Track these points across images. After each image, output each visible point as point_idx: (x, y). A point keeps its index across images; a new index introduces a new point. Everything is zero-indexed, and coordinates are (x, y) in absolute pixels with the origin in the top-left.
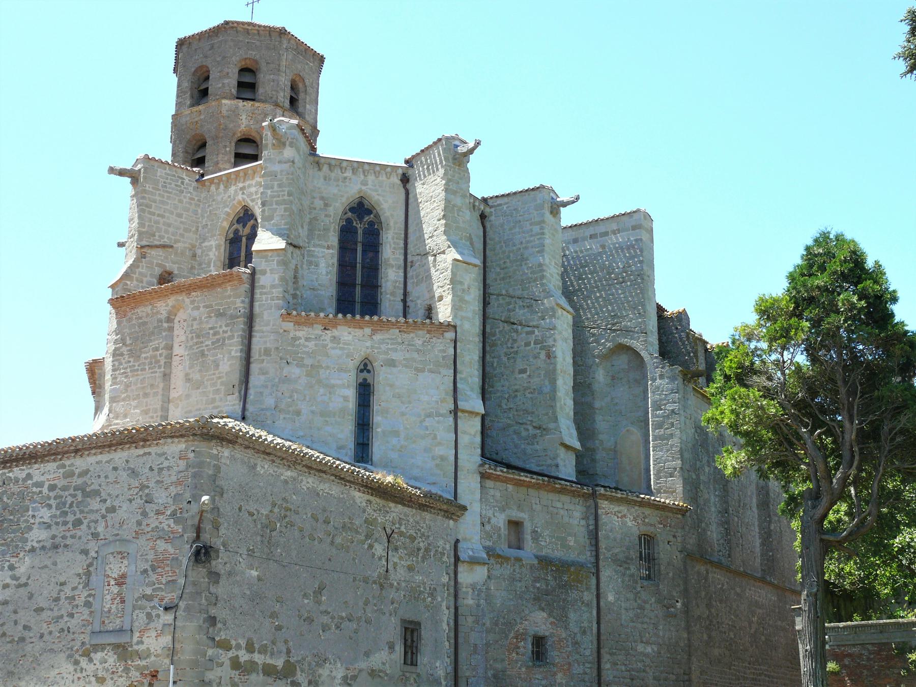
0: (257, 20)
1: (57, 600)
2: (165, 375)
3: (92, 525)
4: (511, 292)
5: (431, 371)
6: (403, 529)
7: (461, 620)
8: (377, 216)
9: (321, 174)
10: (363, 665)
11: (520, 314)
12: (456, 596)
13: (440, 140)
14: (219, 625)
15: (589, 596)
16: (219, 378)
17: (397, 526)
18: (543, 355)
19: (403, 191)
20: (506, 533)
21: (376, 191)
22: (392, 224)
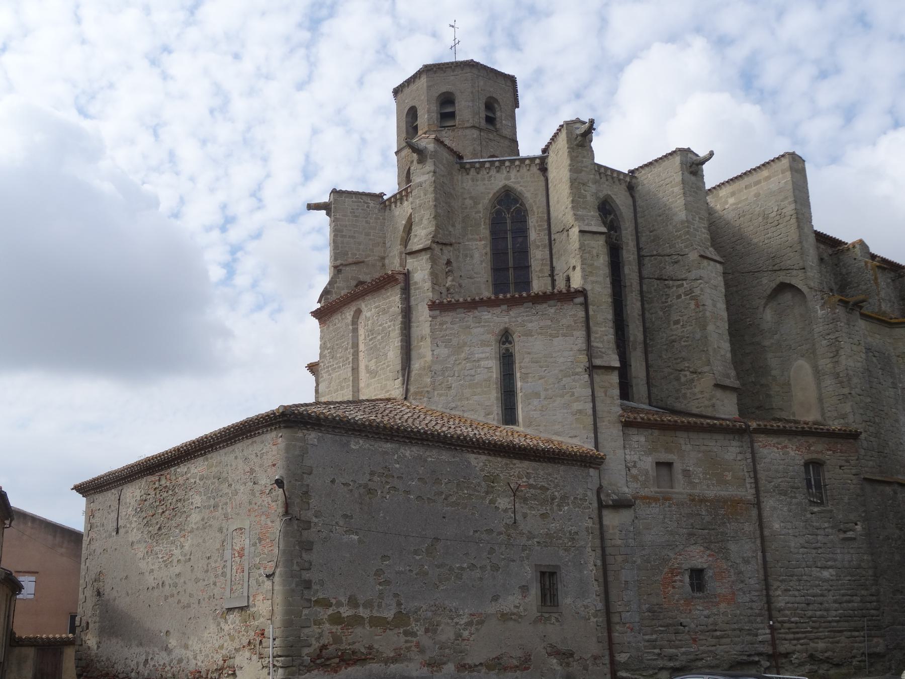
0: (458, 59)
1: (207, 571)
2: (353, 369)
3: (225, 507)
4: (660, 251)
5: (564, 335)
6: (531, 481)
7: (610, 560)
8: (522, 204)
9: (469, 177)
10: (492, 609)
11: (670, 270)
12: (602, 539)
13: (562, 126)
14: (315, 587)
15: (749, 527)
16: (388, 366)
17: (525, 479)
18: (692, 306)
19: (542, 178)
20: (655, 474)
21: (519, 183)
22: (535, 209)
